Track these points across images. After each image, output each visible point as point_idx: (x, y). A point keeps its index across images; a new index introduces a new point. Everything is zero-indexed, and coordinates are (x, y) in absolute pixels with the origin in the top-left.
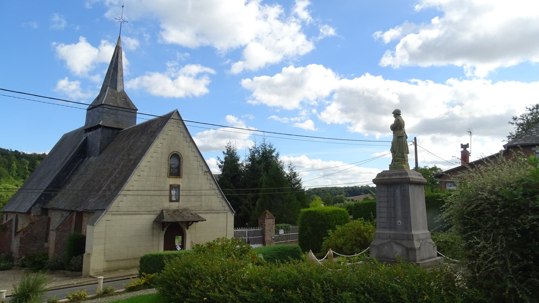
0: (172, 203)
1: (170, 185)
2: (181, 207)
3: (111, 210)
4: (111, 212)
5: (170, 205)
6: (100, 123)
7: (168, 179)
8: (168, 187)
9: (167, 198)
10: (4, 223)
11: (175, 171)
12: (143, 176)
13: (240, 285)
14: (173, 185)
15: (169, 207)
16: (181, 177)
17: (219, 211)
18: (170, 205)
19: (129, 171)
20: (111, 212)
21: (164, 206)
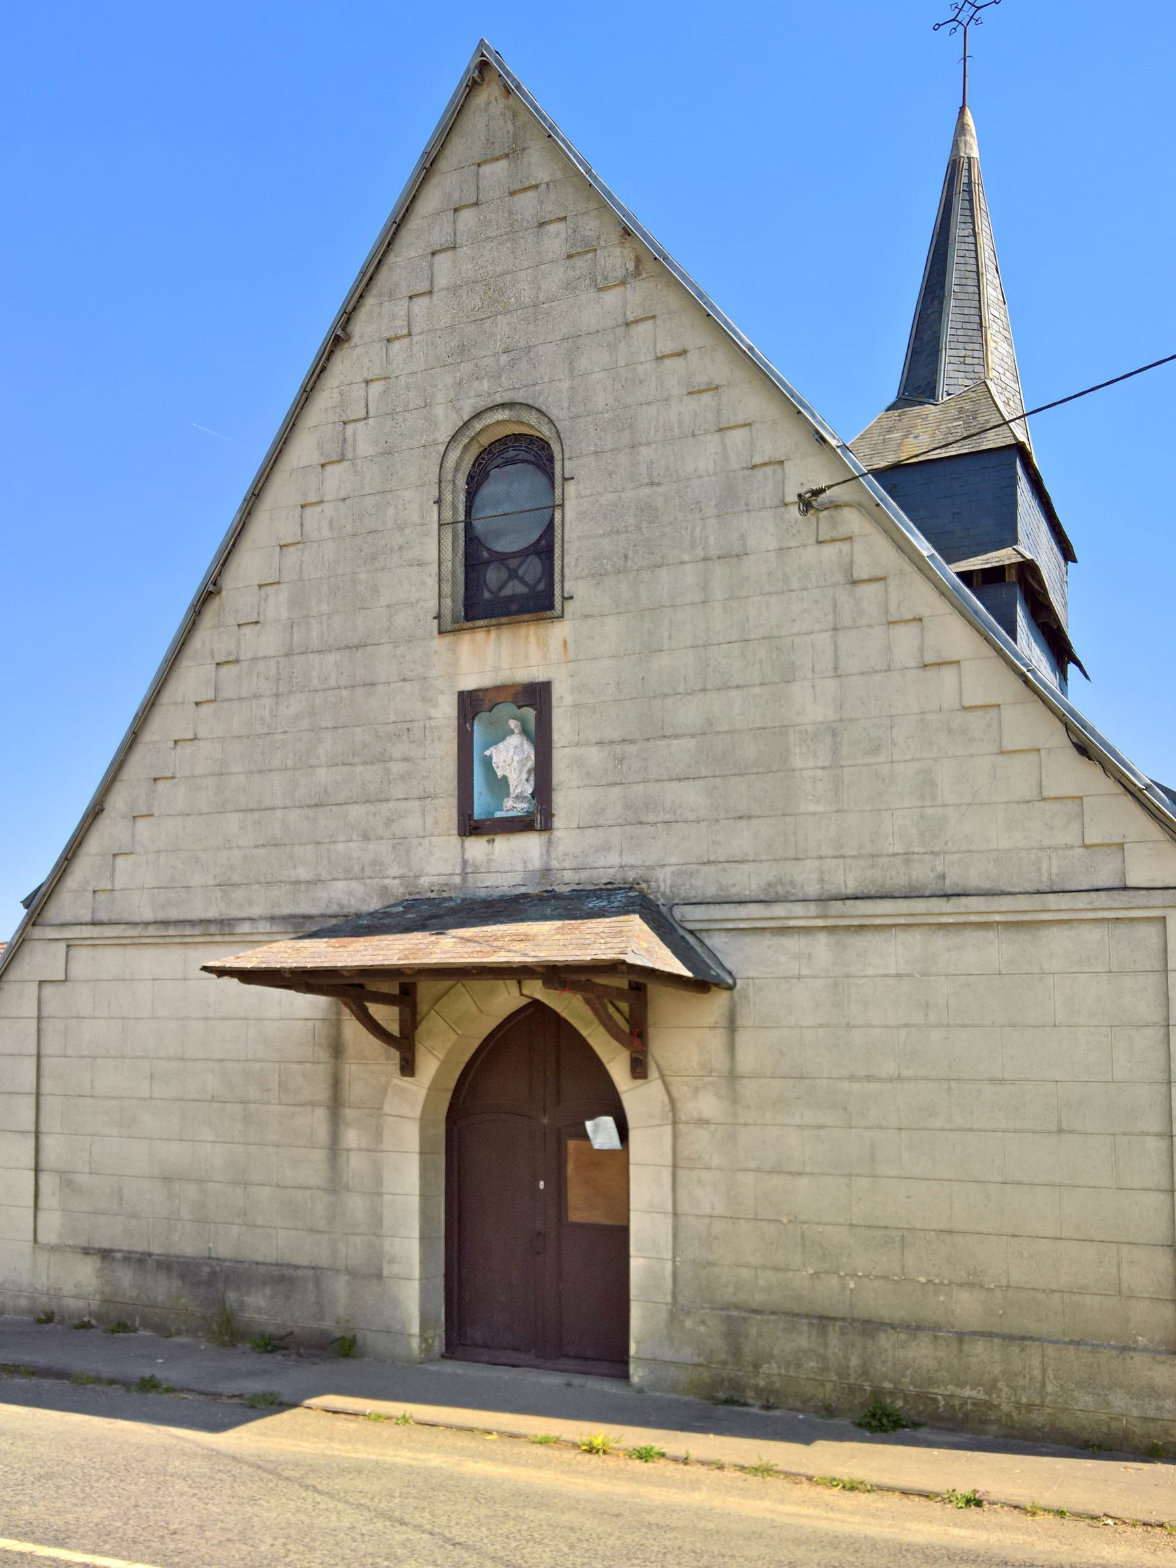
0: (477, 847)
1: (461, 694)
2: (568, 876)
3: (67, 916)
4: (64, 925)
5: (465, 863)
6: (623, 1031)
7: (439, 644)
8: (447, 710)
9: (447, 812)
10: (415, 1328)
11: (521, 580)
12: (254, 659)
13: (512, 1522)
14: (485, 690)
15: (457, 880)
16: (558, 611)
17: (1023, 903)
18: (465, 863)
19: (1091, 1543)
20: (64, 925)
21: (417, 877)
